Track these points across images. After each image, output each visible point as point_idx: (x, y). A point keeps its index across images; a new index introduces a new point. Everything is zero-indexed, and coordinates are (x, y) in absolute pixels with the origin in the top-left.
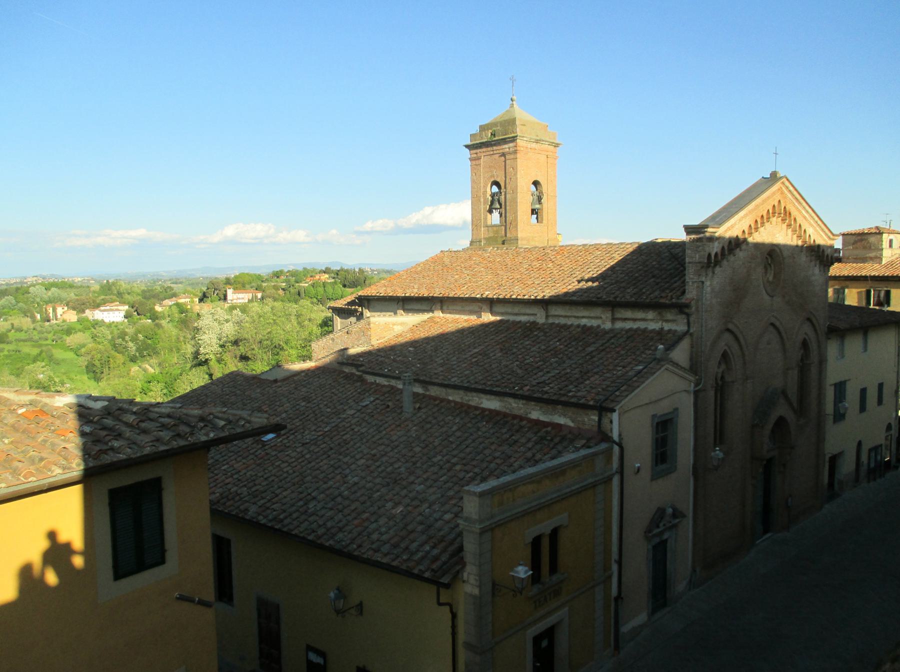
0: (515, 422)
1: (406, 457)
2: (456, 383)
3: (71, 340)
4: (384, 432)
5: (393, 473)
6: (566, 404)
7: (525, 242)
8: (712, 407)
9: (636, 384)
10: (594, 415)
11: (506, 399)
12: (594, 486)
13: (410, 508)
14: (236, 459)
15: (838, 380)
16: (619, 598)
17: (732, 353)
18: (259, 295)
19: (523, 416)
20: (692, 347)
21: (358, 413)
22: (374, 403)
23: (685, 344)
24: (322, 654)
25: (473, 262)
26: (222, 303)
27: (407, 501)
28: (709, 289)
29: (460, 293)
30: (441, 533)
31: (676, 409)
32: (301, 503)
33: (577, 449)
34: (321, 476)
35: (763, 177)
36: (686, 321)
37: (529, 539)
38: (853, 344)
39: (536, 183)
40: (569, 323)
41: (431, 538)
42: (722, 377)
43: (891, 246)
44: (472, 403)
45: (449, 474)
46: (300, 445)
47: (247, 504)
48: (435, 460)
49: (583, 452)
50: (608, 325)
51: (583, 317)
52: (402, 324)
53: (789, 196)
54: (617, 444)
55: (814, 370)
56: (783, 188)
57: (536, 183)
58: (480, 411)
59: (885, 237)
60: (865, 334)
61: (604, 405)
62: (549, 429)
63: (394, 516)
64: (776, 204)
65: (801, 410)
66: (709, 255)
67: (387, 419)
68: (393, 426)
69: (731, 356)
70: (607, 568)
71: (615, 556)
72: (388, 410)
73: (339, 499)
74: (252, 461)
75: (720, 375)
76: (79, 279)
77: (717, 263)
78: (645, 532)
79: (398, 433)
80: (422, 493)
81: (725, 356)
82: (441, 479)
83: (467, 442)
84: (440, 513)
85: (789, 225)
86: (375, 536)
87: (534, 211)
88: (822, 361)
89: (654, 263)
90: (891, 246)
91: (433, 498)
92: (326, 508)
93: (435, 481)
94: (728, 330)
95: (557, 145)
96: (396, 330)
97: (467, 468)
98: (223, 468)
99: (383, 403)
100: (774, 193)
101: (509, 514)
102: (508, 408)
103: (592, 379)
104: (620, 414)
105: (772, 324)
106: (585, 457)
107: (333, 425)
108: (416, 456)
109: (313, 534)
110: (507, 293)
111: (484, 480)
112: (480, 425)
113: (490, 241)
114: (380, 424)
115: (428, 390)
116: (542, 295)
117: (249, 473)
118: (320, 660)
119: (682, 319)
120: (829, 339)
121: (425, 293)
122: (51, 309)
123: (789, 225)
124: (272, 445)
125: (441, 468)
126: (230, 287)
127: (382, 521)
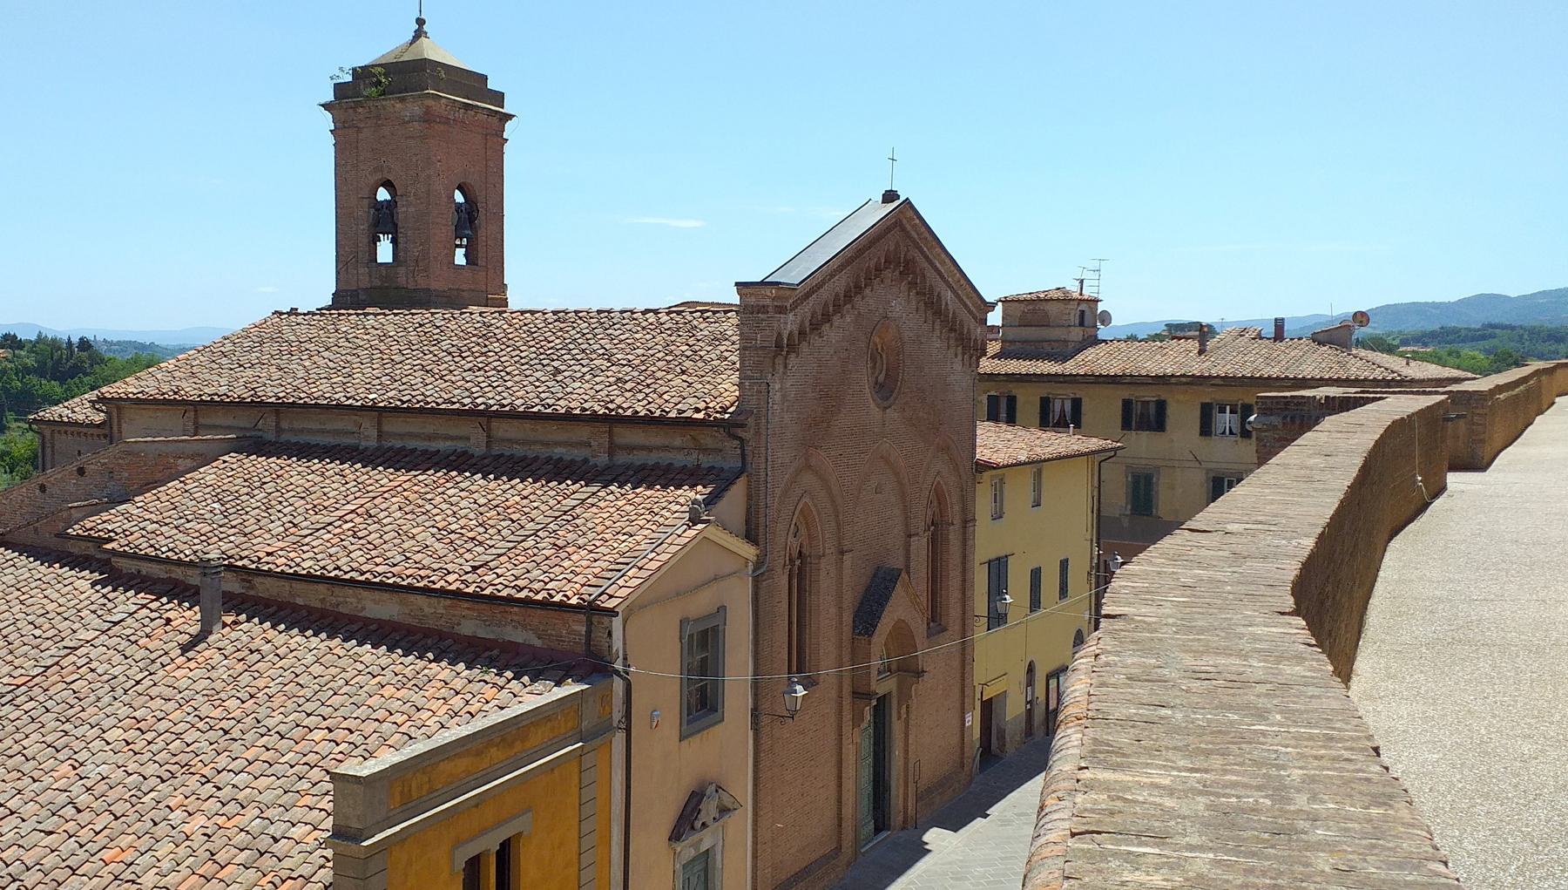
15: (993, 556)
21: (103, 637)
28: (778, 397)
31: (722, 609)
40: (531, 455)
50: (104, 390)
51: (557, 444)
60: (1296, 612)
66: (779, 335)
77: (792, 348)
85: (913, 284)
88: (968, 521)
127: (164, 848)
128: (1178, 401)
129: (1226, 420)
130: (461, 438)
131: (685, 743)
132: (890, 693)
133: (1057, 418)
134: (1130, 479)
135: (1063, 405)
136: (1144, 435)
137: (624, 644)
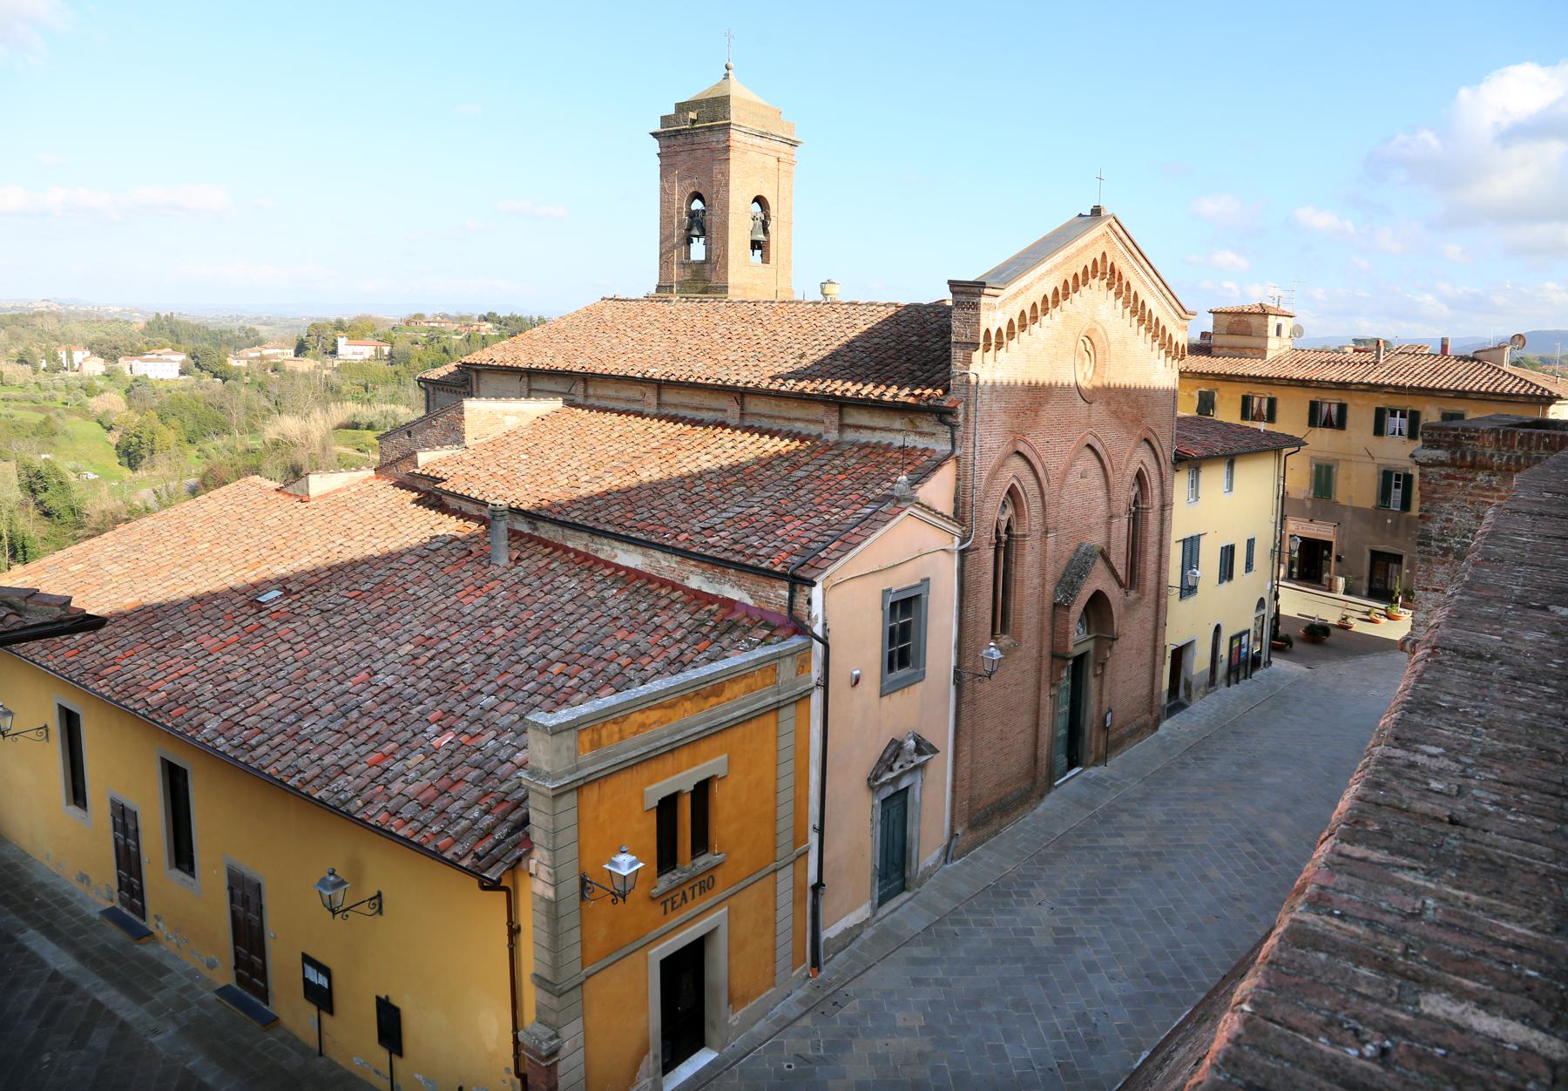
0: (663, 592)
1: (478, 644)
2: (577, 520)
3: (96, 404)
4: (454, 598)
5: (453, 671)
6: (741, 567)
7: (738, 292)
8: (990, 577)
9: (855, 540)
10: (784, 588)
11: (651, 552)
12: (777, 708)
13: (464, 738)
14: (209, 632)
15: (1187, 535)
16: (818, 887)
17: (1024, 491)
18: (387, 349)
19: (677, 582)
20: (958, 479)
22: (449, 547)
23: (947, 473)
24: (324, 970)
25: (645, 319)
26: (329, 359)
27: (463, 724)
29: (611, 368)
30: (504, 787)
32: (292, 718)
33: (753, 645)
34: (335, 671)
35: (1080, 215)
36: (949, 436)
37: (653, 802)
38: (1213, 477)
39: (759, 200)
41: (486, 794)
42: (1008, 529)
43: (1278, 334)
44: (602, 556)
45: (541, 679)
46: (318, 612)
47: (206, 715)
48: (524, 652)
49: (760, 652)
51: (797, 419)
52: (517, 414)
53: (1119, 245)
54: (818, 639)
55: (1153, 517)
56: (1111, 234)
57: (759, 200)
58: (612, 570)
59: (1272, 322)
60: (1231, 465)
61: (799, 573)
62: (715, 607)
63: (436, 750)
64: (1099, 258)
65: (1132, 580)
67: (463, 576)
68: (472, 588)
69: (1023, 495)
70: (800, 838)
71: (814, 820)
72: (470, 558)
73: (355, 714)
74: (235, 637)
75: (1004, 526)
76: (117, 309)
78: (869, 779)
79: (475, 601)
80: (489, 711)
81: (1012, 493)
82: (525, 688)
83: (579, 624)
84: (510, 750)
86: (396, 787)
87: (755, 245)
88: (1165, 506)
89: (914, 338)
90: (1278, 334)
91: (506, 721)
92: (330, 730)
93: (517, 690)
94: (1018, 453)
95: (794, 144)
96: (507, 424)
97: (568, 670)
98: (185, 647)
99: (463, 546)
100: (1095, 240)
101: (612, 761)
102: (654, 568)
103: (789, 527)
104: (824, 590)
105: (1089, 446)
106: (759, 662)
107: (377, 580)
108: (496, 643)
109: (298, 776)
110: (682, 372)
111: (594, 693)
112: (607, 594)
113: (686, 287)
114: (452, 582)
115: (536, 529)
116: (734, 379)
117: (223, 658)
118: (323, 981)
119: (943, 432)
120: (1177, 471)
121: (560, 364)
122: (64, 353)
123: (1118, 294)
124: (273, 609)
125: (530, 668)
126: (342, 334)
127: (417, 757)
128: (1356, 405)
129: (1396, 423)
130: (720, 410)
131: (886, 699)
132: (1087, 652)
133: (1323, 419)
134: (1314, 468)
135: (1329, 409)
136: (1327, 431)
137: (824, 610)
